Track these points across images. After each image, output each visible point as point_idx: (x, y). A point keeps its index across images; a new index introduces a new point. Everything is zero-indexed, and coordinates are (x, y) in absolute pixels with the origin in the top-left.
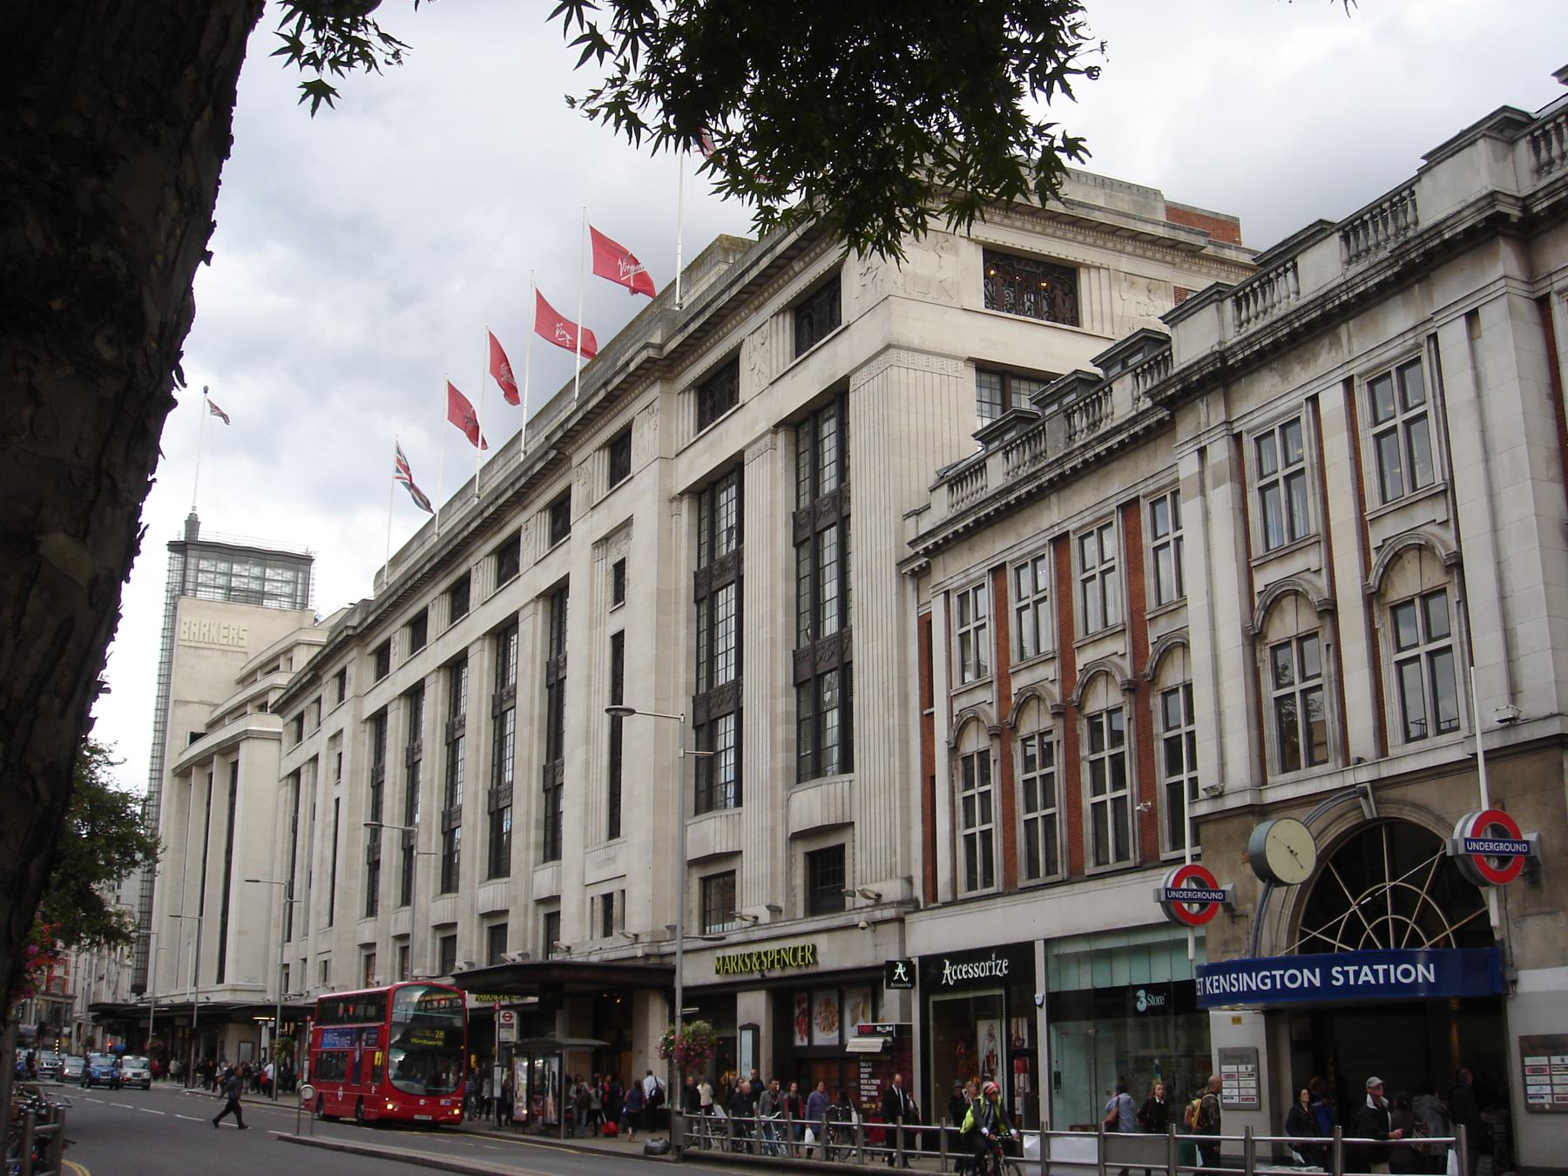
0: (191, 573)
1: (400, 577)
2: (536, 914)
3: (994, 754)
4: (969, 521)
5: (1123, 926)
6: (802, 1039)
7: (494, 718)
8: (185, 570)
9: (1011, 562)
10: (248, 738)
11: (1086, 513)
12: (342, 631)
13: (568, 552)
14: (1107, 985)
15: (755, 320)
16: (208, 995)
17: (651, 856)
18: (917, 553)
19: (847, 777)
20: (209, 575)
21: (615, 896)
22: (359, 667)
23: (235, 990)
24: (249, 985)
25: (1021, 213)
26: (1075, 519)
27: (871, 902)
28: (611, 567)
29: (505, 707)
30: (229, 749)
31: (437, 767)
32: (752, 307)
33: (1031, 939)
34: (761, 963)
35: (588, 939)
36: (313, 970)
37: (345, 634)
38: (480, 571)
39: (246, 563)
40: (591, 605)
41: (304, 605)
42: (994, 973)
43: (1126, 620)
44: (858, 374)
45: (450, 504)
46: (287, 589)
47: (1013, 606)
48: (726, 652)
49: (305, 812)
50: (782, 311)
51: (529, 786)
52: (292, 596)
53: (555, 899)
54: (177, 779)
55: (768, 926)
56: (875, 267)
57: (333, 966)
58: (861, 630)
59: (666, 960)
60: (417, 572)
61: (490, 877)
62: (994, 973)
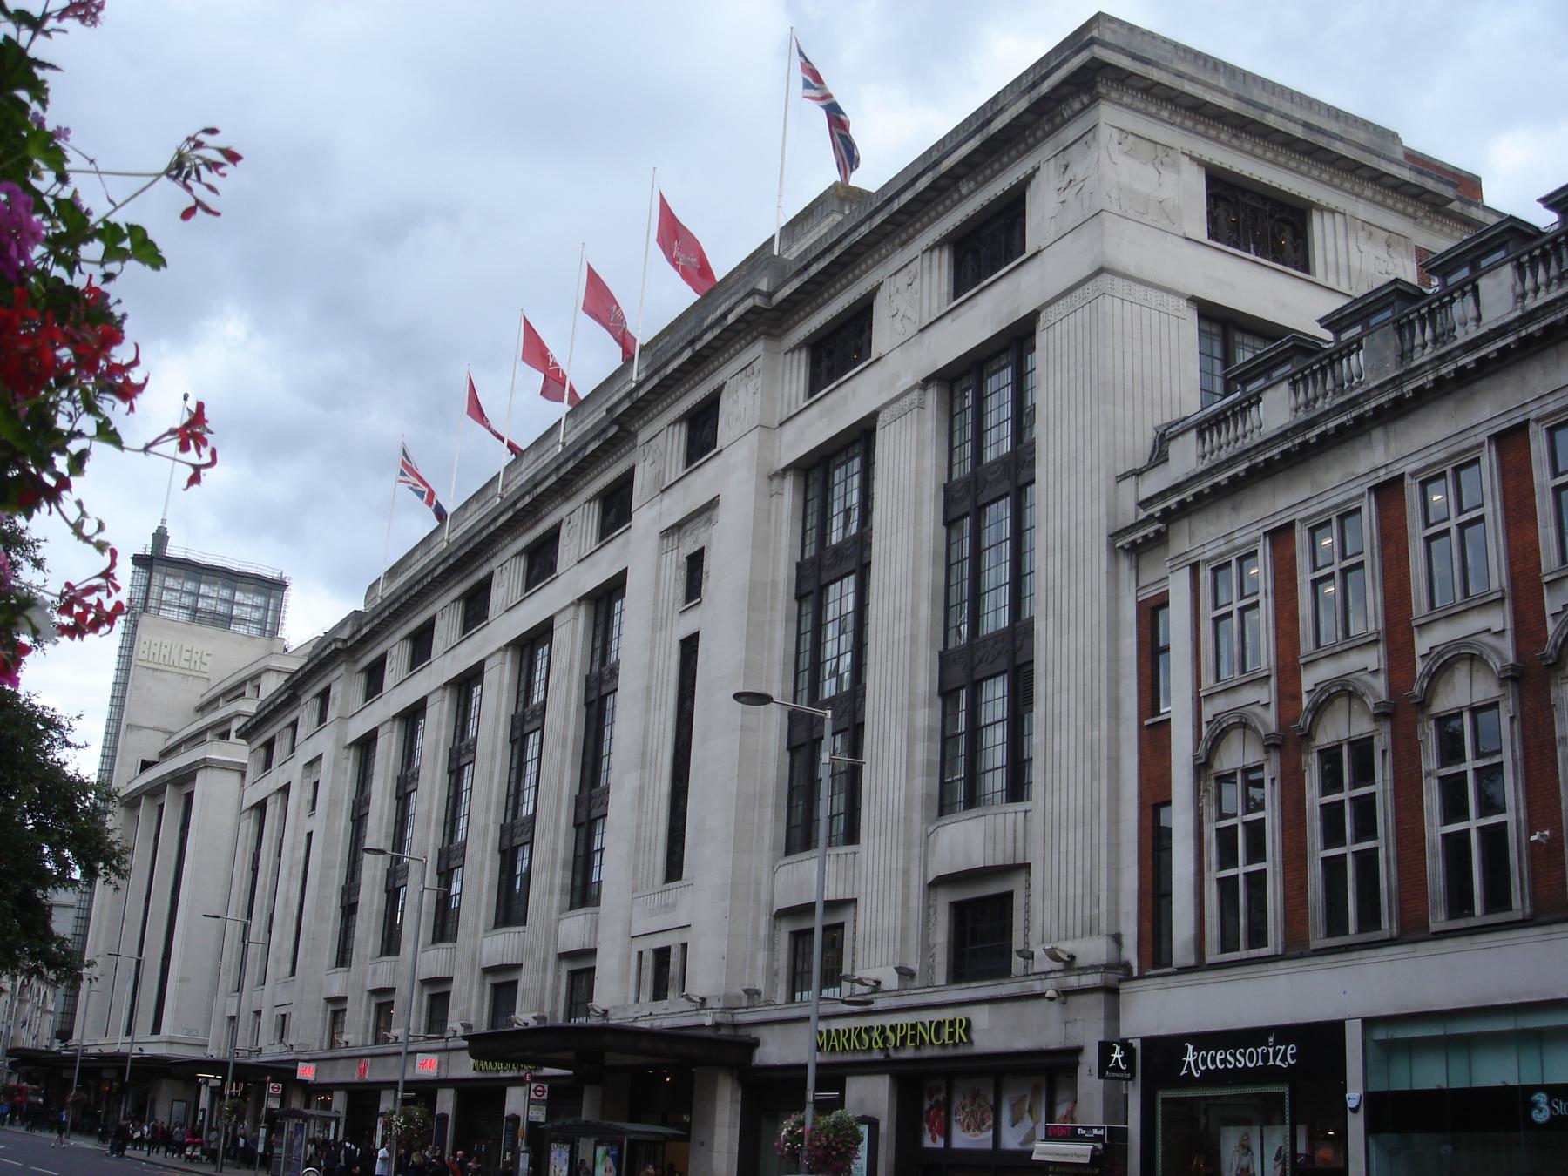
0: (155, 590)
1: (405, 583)
2: (557, 971)
3: (1382, 742)
4: (1239, 469)
5: (1508, 1001)
6: (934, 1140)
7: (513, 741)
8: (149, 586)
9: (1303, 520)
10: (206, 767)
11: (1435, 449)
12: (330, 644)
13: (626, 544)
14: (1463, 1084)
15: (898, 259)
16: (141, 1046)
17: (728, 902)
18: (1152, 516)
19: (1020, 806)
20: (174, 594)
21: (673, 951)
22: (345, 686)
23: (172, 1043)
24: (190, 1039)
25: (1252, 134)
26: (1415, 458)
27: (1059, 965)
28: (684, 560)
29: (463, 761)
30: (184, 778)
31: (436, 798)
32: (897, 241)
33: (1339, 1017)
34: (886, 1040)
35: (631, 1001)
36: (268, 1025)
37: (333, 647)
38: (505, 577)
39: (215, 583)
40: (655, 604)
41: (274, 633)
42: (1271, 1062)
43: (1505, 584)
44: (1052, 308)
45: (465, 506)
46: (257, 615)
47: (1304, 577)
48: (838, 656)
49: (270, 848)
51: (557, 820)
52: (262, 623)
53: (591, 953)
54: (123, 808)
55: (899, 992)
56: (1079, 178)
57: (293, 1022)
58: (1050, 621)
59: (742, 1032)
60: (427, 575)
61: (497, 925)
62: (1271, 1062)
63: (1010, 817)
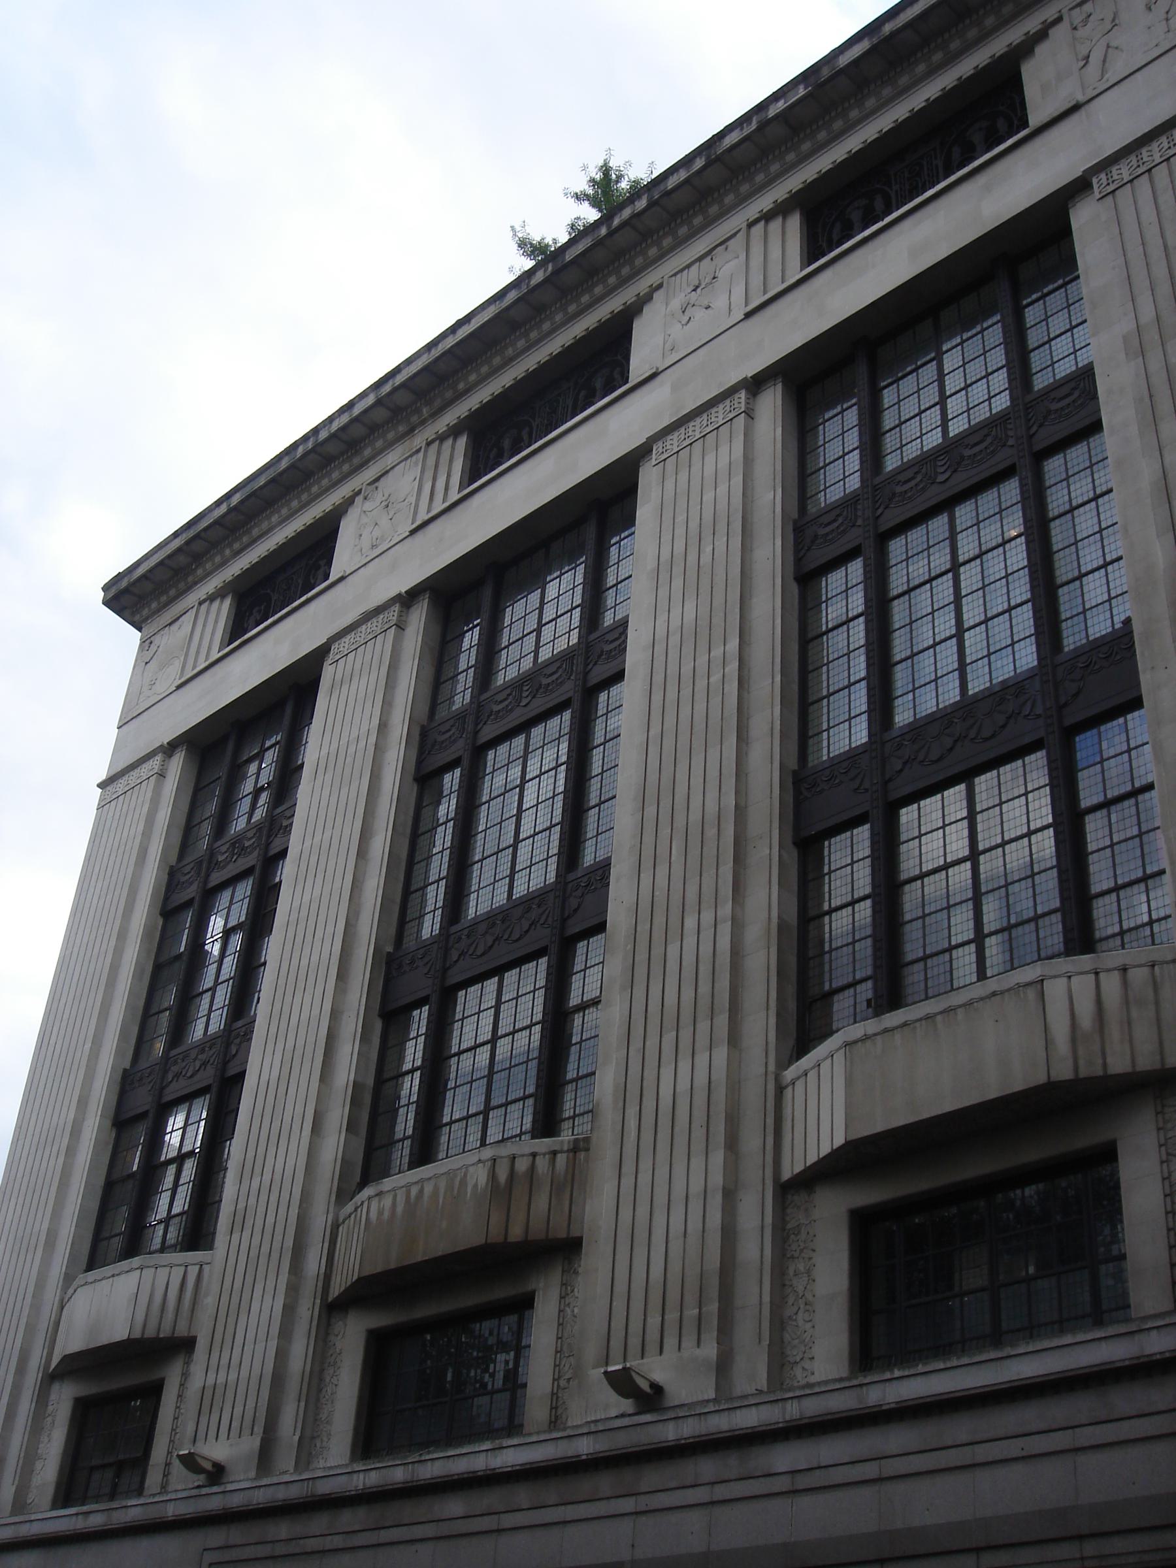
50: (781, 210)
63: (177, 1273)
